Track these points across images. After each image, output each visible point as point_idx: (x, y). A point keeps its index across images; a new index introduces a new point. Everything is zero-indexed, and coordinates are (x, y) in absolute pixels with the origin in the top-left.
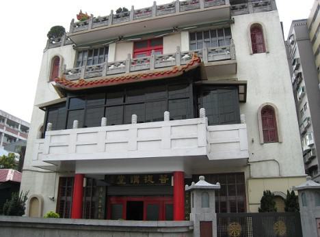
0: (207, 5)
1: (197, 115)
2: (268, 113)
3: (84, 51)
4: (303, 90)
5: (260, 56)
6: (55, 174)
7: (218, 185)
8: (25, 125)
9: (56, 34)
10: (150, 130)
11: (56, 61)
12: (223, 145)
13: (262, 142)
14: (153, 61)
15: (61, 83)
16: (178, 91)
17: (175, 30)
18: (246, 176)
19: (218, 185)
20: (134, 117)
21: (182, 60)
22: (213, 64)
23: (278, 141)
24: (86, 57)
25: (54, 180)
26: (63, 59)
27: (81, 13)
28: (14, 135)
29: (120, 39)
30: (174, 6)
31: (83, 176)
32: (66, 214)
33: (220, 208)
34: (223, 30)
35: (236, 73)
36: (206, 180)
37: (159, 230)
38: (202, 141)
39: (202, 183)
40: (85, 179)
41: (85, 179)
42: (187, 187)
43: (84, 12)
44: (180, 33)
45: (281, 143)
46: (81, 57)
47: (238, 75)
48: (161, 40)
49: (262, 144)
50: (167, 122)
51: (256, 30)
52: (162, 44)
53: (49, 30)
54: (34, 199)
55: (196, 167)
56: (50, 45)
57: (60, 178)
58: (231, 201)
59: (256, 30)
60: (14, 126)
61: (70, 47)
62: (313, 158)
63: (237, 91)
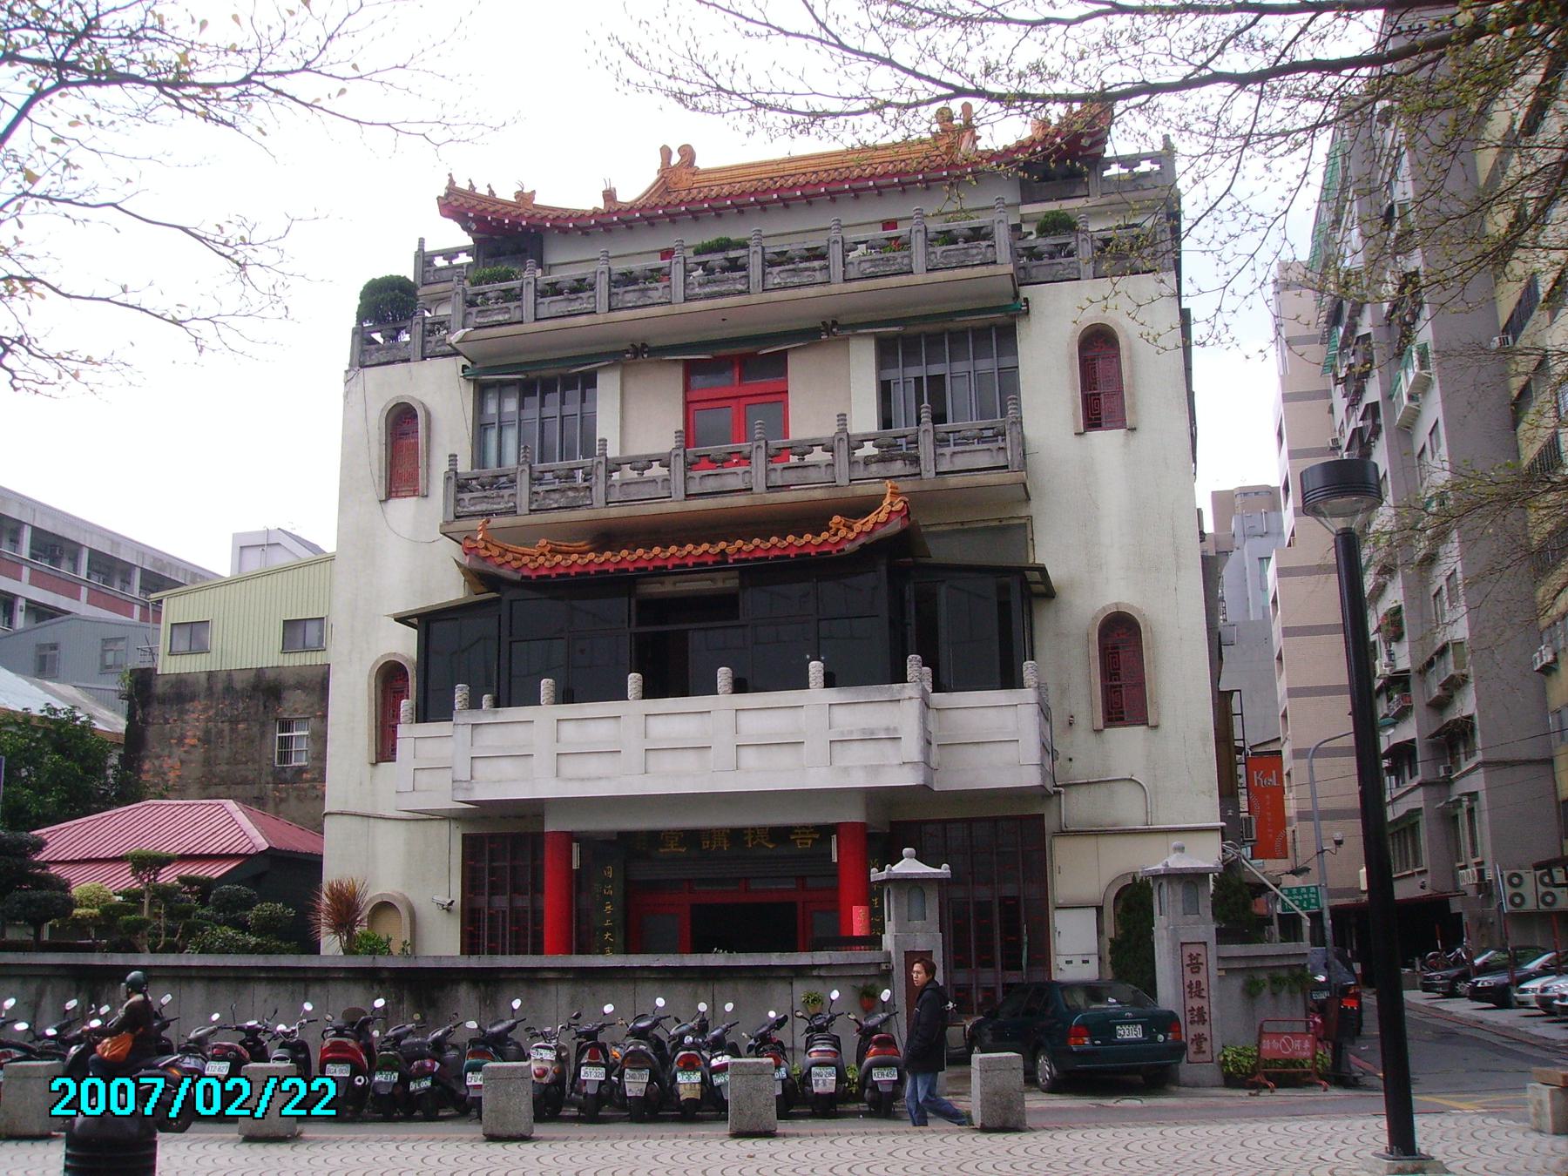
0: (937, 259)
1: (901, 677)
2: (1120, 637)
3: (501, 386)
4: (1423, 364)
5: (1105, 440)
6: (445, 825)
7: (945, 870)
8: (48, 526)
9: (389, 309)
10: (767, 714)
11: (403, 422)
12: (975, 748)
13: (1100, 723)
14: (759, 459)
15: (485, 559)
16: (848, 141)
17: (825, 332)
18: (1050, 824)
19: (945, 870)
20: (724, 675)
21: (852, 463)
22: (953, 481)
23: (1145, 722)
24: (511, 405)
25: (447, 848)
26: (428, 414)
27: (452, 190)
28: (62, 602)
29: (635, 354)
30: (823, 257)
31: (571, 837)
32: (533, 944)
33: (956, 926)
34: (995, 328)
35: (1028, 499)
36: (920, 857)
37: (815, 973)
38: (911, 748)
39: (909, 866)
40: (575, 847)
41: (575, 847)
42: (876, 875)
43: (463, 185)
44: (847, 339)
45: (1156, 727)
46: (492, 408)
47: (1033, 503)
48: (782, 357)
49: (1098, 731)
50: (817, 695)
51: (1097, 348)
52: (784, 372)
53: (356, 302)
54: (384, 907)
55: (894, 820)
56: (365, 354)
57: (466, 838)
58: (1003, 900)
59: (1097, 348)
60: (55, 560)
61: (452, 366)
62: (1454, 685)
63: (1021, 593)
